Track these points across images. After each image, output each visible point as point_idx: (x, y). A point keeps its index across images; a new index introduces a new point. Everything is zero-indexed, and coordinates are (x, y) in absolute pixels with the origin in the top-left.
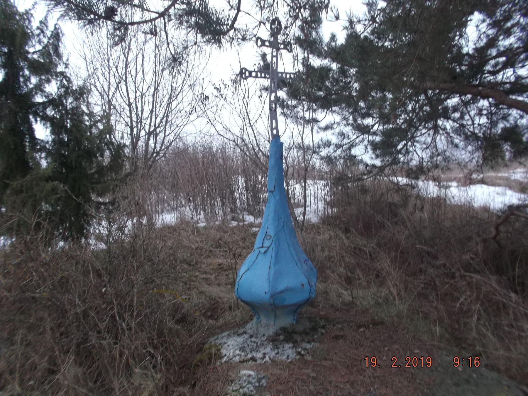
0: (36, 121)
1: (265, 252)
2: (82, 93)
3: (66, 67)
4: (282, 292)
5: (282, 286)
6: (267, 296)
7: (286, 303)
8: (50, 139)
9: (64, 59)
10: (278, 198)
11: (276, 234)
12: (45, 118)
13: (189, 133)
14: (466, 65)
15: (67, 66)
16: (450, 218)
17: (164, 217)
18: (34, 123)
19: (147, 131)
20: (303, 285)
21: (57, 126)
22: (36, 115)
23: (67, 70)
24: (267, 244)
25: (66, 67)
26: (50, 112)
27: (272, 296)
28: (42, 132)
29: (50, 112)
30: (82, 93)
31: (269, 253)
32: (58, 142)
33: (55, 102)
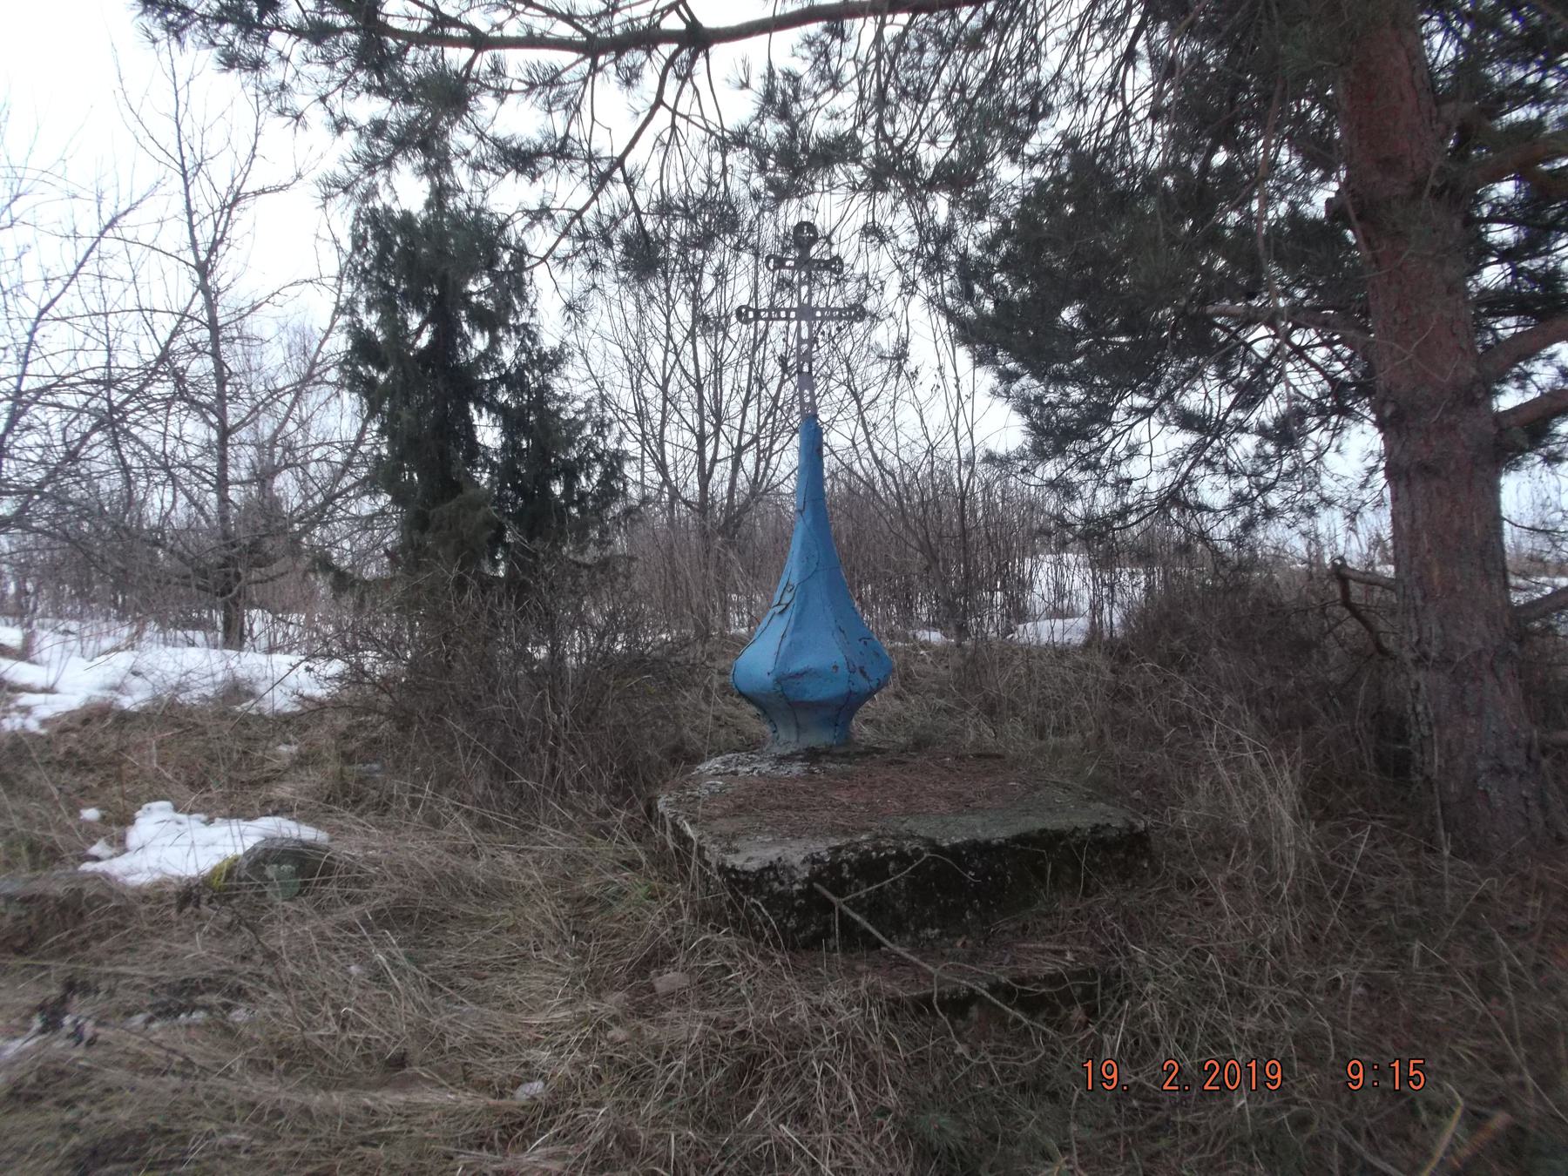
0: (480, 411)
1: (782, 612)
2: (553, 361)
3: (532, 315)
4: (798, 675)
5: (798, 666)
6: (770, 679)
7: (807, 697)
8: (498, 444)
9: (531, 300)
10: (809, 521)
11: (802, 583)
12: (493, 407)
13: (246, 304)
14: (1312, 108)
15: (533, 312)
16: (548, 387)
17: (136, 358)
18: (476, 417)
19: (735, 444)
20: (836, 667)
21: (512, 422)
22: (479, 403)
23: (532, 321)
24: (787, 598)
25: (532, 315)
26: (503, 396)
27: (778, 681)
28: (489, 433)
29: (503, 396)
30: (553, 361)
31: (787, 615)
32: (510, 447)
33: (514, 381)
